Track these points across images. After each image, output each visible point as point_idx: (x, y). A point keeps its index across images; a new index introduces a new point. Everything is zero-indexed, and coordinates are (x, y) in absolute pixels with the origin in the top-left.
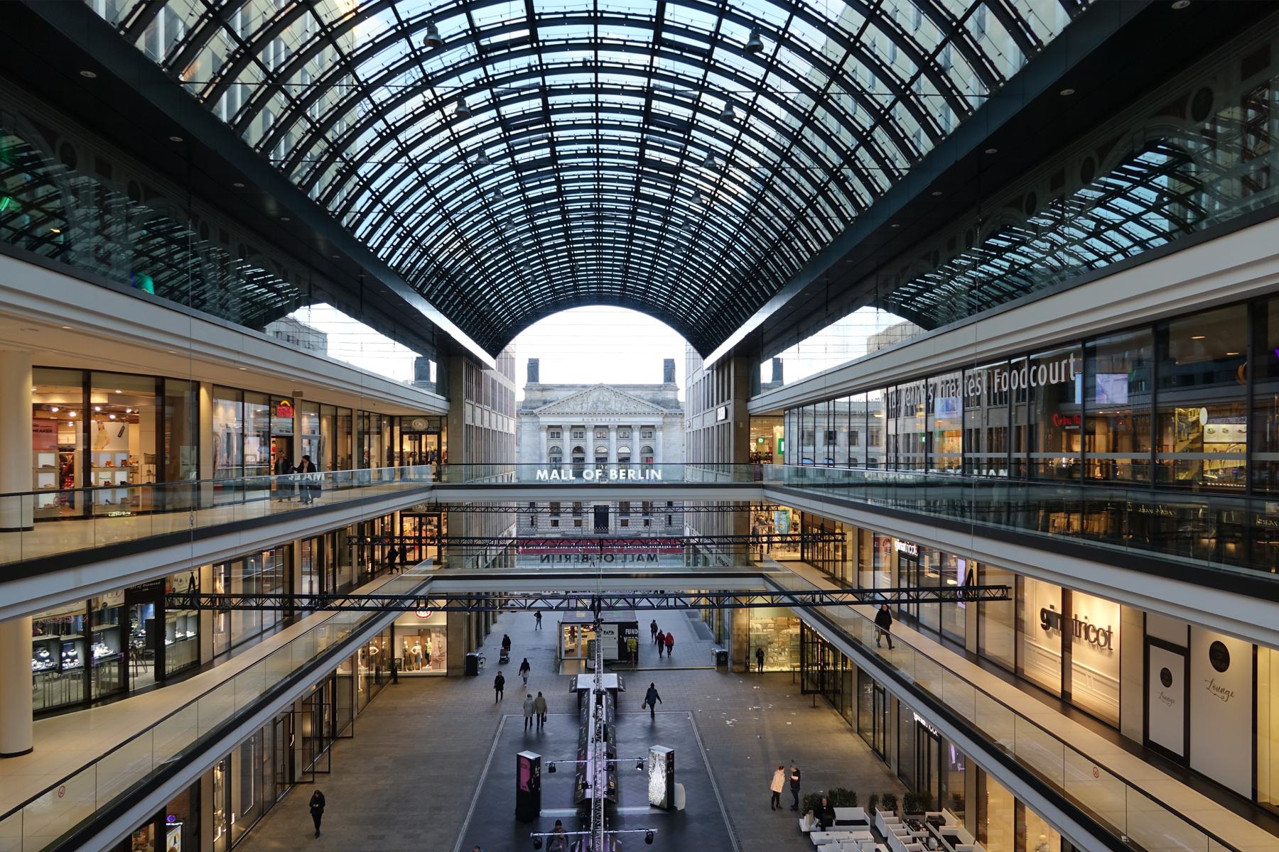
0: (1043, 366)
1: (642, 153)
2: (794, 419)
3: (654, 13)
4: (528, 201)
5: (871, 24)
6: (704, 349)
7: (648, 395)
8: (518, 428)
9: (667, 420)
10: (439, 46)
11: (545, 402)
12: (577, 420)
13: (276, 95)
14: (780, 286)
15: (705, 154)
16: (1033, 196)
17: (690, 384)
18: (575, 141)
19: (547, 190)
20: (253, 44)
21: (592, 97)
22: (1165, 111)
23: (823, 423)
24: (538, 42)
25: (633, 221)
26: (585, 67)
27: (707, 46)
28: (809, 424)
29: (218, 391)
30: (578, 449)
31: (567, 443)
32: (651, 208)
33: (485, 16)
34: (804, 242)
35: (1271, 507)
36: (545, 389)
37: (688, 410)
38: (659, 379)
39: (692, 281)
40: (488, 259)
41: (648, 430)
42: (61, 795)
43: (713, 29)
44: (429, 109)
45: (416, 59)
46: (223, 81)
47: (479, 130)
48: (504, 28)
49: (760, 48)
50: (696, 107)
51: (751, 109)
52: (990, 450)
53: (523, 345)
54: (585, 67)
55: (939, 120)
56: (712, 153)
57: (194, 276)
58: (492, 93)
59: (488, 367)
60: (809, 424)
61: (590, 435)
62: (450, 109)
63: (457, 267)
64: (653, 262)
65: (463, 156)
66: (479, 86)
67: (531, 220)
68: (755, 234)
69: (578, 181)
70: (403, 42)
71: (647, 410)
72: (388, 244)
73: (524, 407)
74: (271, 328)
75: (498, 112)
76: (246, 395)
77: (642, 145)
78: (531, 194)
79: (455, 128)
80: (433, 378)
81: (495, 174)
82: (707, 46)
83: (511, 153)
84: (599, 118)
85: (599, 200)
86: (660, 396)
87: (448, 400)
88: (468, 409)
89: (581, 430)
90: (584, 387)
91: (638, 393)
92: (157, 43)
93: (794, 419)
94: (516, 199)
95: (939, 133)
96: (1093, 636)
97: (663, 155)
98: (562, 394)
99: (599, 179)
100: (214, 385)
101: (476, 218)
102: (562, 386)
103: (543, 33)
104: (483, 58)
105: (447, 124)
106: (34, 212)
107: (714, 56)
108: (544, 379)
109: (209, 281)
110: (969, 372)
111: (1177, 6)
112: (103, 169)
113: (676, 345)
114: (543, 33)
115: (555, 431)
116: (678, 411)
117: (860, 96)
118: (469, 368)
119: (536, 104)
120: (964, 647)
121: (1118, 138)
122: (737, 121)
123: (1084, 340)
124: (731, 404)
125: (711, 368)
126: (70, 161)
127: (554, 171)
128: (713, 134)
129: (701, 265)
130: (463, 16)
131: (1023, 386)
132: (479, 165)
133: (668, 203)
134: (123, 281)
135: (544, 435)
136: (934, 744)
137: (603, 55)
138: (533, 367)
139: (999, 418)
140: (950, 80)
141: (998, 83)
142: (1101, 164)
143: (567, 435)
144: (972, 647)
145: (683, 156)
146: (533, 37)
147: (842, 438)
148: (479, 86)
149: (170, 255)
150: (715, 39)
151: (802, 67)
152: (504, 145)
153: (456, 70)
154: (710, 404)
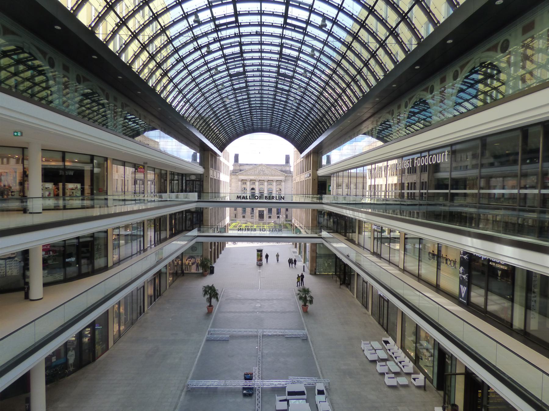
0: (434, 156)
1: (279, 71)
2: (335, 178)
3: (284, 12)
4: (234, 90)
5: (370, 15)
6: (301, 151)
7: (280, 168)
8: (28, 93)
10: (199, 23)
11: (241, 171)
12: (252, 177)
13: (134, 42)
14: (326, 130)
15: (303, 71)
17: (295, 164)
18: (253, 65)
19: (244, 97)
21: (260, 61)
22: (489, 50)
23: (346, 180)
25: (275, 99)
26: (257, 34)
28: (340, 180)
29: (116, 161)
30: (253, 189)
31: (248, 186)
32: (280, 104)
33: (218, 11)
34: (340, 107)
35: (547, 217)
37: (294, 174)
38: (284, 162)
39: (297, 123)
40: (221, 115)
41: (279, 182)
43: (307, 18)
44: (196, 50)
45: (191, 29)
47: (222, 78)
48: (225, 17)
49: (325, 26)
50: (300, 51)
51: (322, 52)
52: (408, 189)
53: (233, 148)
54: (257, 34)
56: (306, 70)
57: (103, 116)
59: (219, 156)
60: (340, 180)
61: (257, 183)
62: (204, 50)
63: (207, 116)
64: (284, 108)
65: (209, 70)
66: (215, 41)
67: (236, 97)
68: (322, 104)
69: (253, 78)
70: (185, 21)
71: (279, 174)
73: (233, 172)
74: (137, 139)
75: (223, 52)
76: (126, 164)
77: (279, 67)
78: (236, 87)
79: (206, 58)
80: (198, 160)
81: (222, 77)
83: (232, 85)
84: (261, 60)
85: (262, 90)
86: (284, 169)
87: (204, 168)
88: (211, 172)
90: (255, 165)
92: (85, 17)
93: (335, 178)
94: (233, 100)
96: (449, 262)
97: (287, 71)
98: (247, 167)
99: (262, 86)
100: (113, 159)
101: (215, 95)
102: (247, 164)
103: (241, 19)
104: (217, 29)
105: (203, 56)
106: (17, 78)
107: (308, 30)
108: (241, 161)
110: (431, 153)
111: (498, 3)
113: (289, 148)
114: (245, 55)
115: (244, 182)
116: (291, 175)
118: (212, 156)
119: (237, 49)
120: (398, 267)
122: (315, 57)
123: (451, 145)
124: (311, 172)
125: (303, 157)
127: (246, 91)
128: (300, 80)
129: (300, 116)
130: (209, 11)
131: (426, 164)
132: (222, 89)
133: (288, 91)
135: (240, 183)
136: (386, 303)
137: (264, 29)
138: (236, 157)
139: (413, 178)
140: (401, 39)
141: (421, 39)
142: (461, 72)
143: (248, 183)
144: (401, 267)
145: (294, 71)
146: (237, 21)
147: (353, 186)
148: (215, 41)
149: (99, 109)
150: (308, 22)
151: (338, 45)
153: (206, 34)
154: (302, 172)
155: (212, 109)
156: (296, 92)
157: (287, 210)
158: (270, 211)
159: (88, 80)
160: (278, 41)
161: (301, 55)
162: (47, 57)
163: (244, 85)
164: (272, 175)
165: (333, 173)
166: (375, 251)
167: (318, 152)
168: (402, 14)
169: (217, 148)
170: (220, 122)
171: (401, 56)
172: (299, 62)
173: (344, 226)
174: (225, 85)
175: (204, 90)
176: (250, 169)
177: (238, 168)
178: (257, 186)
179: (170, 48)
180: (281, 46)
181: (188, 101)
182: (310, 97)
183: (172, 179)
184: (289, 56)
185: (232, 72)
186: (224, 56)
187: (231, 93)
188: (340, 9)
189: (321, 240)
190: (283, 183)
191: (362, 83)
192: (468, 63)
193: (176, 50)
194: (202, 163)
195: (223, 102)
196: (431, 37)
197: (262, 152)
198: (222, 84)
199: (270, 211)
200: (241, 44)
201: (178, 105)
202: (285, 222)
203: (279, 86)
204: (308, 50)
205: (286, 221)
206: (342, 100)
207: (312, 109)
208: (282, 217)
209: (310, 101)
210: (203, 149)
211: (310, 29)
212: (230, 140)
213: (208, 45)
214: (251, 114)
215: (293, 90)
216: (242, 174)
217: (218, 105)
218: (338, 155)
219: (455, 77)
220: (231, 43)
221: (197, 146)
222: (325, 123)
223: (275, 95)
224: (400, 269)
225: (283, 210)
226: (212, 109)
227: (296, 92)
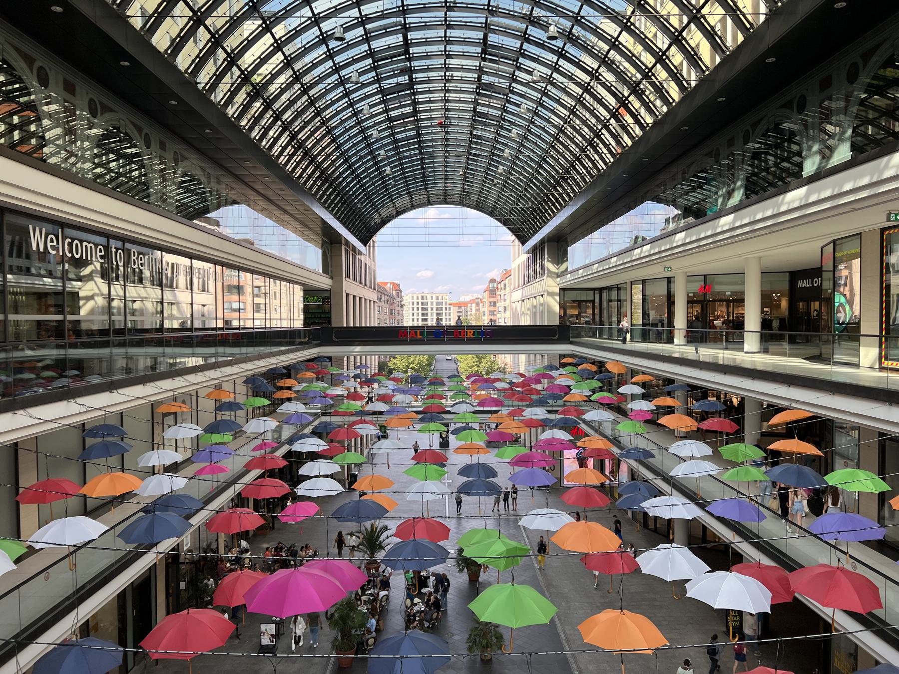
1: (479, 78)
6: (523, 240)
16: (718, 149)
20: (235, 55)
24: (409, 54)
42: (47, 579)
46: (200, 62)
55: (749, 17)
58: (365, 29)
59: (360, 253)
72: (285, 154)
77: (481, 70)
78: (393, 114)
95: (748, 26)
109: (52, 142)
112: (69, 88)
117: (631, 58)
119: (404, 79)
121: (761, 119)
125: (528, 252)
126: (44, 82)
134: (172, 212)
141: (704, 72)
142: (864, 66)
152: (374, 74)
159: (111, 110)
162: (36, 65)
163: (409, 110)
168: (692, 11)
169: (356, 237)
171: (693, 78)
172: (521, 60)
182: (543, 129)
185: (386, 84)
186: (371, 54)
192: (878, 46)
194: (326, 269)
196: (740, 48)
203: (480, 109)
206: (588, 156)
207: (561, 130)
209: (543, 134)
210: (331, 243)
214: (423, 168)
217: (358, 152)
219: (852, 78)
220: (385, 27)
221: (317, 234)
224: (609, 440)
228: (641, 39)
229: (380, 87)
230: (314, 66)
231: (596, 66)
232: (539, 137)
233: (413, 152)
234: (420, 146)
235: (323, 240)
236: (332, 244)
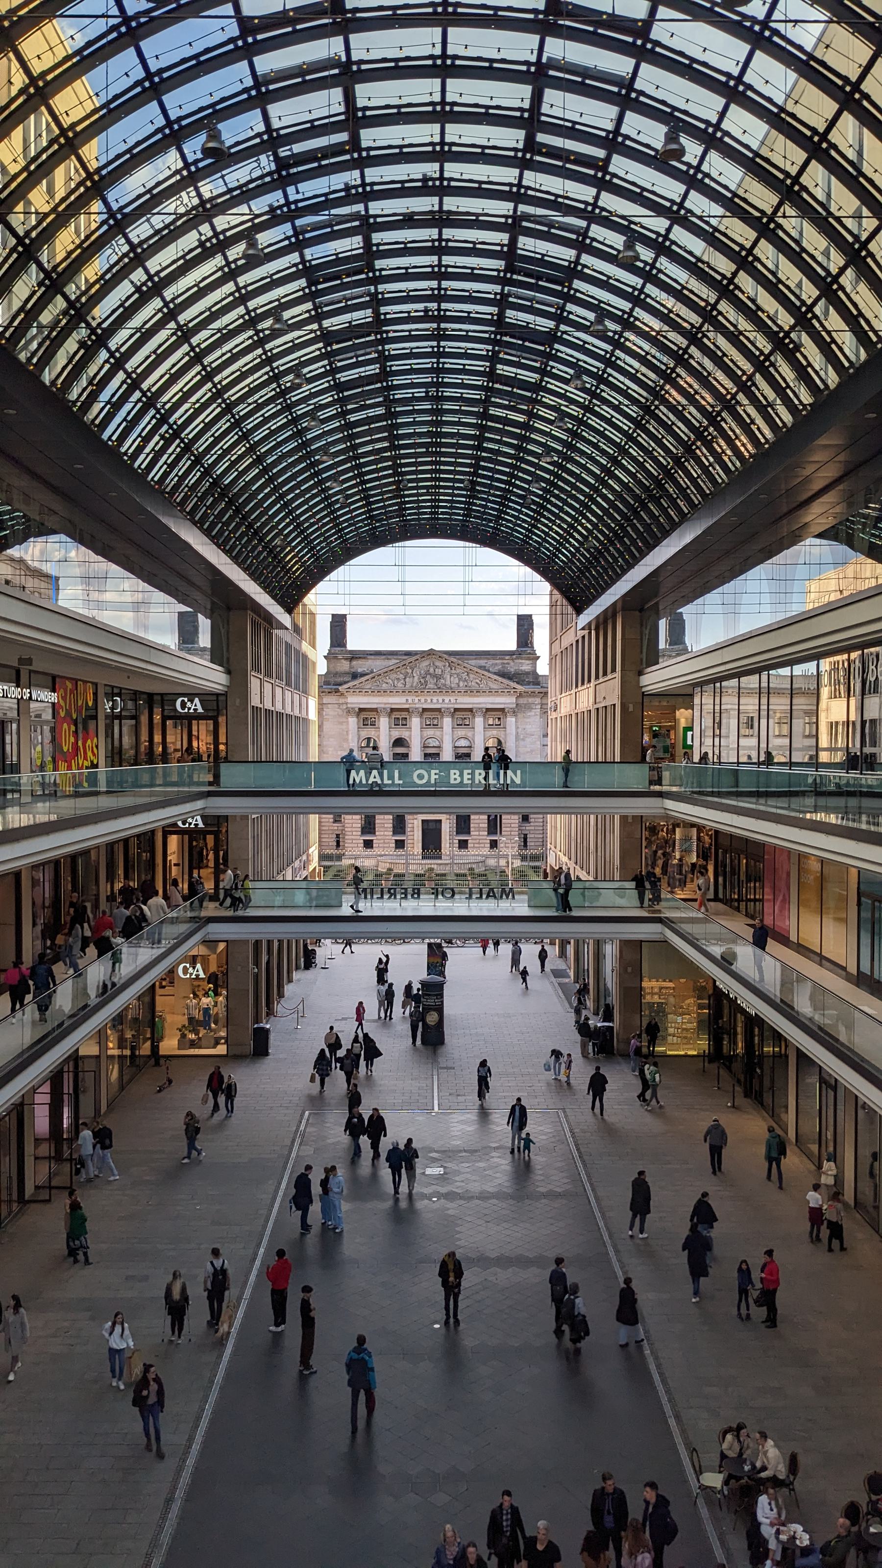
1: (501, 315)
2: (708, 700)
3: (526, 105)
7: (497, 664)
9: (522, 701)
11: (355, 676)
12: (397, 701)
15: (591, 316)
17: (557, 649)
18: (408, 299)
24: (374, 271)
27: (601, 153)
31: (384, 734)
36: (356, 656)
39: (565, 502)
43: (610, 126)
44: (206, 252)
49: (680, 153)
50: (582, 244)
58: (294, 227)
61: (415, 722)
62: (236, 252)
65: (252, 321)
66: (275, 218)
71: (494, 686)
73: (327, 683)
77: (502, 302)
80: (204, 640)
82: (601, 153)
85: (438, 385)
86: (513, 667)
87: (228, 672)
89: (404, 714)
90: (408, 654)
91: (482, 662)
93: (708, 700)
98: (377, 664)
99: (438, 371)
103: (369, 137)
104: (284, 176)
105: (231, 274)
107: (612, 169)
108: (353, 643)
115: (367, 717)
116: (537, 689)
119: (352, 244)
125: (588, 626)
129: (578, 477)
132: (275, 334)
135: (353, 721)
138: (339, 624)
143: (384, 722)
146: (355, 142)
148: (275, 218)
152: (309, 305)
155: (245, 436)
156: (549, 431)
157: (525, 818)
158: (463, 824)
160: (502, 208)
161: (586, 259)
164: (469, 692)
165: (701, 684)
166: (866, 968)
167: (643, 606)
170: (299, 525)
172: (577, 284)
173: (741, 875)
174: (286, 315)
175: (233, 394)
176: (388, 672)
177: (344, 666)
178: (415, 734)
179: (93, 217)
180: (514, 226)
181: (176, 434)
183: (121, 710)
184: (542, 261)
185: (333, 323)
187: (326, 399)
188: (761, 37)
189: (657, 928)
190: (511, 720)
191: (811, 352)
193: (97, 184)
194: (219, 654)
195: (300, 433)
197: (439, 599)
198: (295, 370)
199: (463, 824)
200: (367, 226)
201: (139, 450)
202: (518, 863)
204: (651, 133)
205: (524, 858)
208: (509, 844)
210: (225, 603)
211: (620, 165)
212: (320, 569)
213: (248, 235)
215: (554, 385)
216: (360, 691)
218: (713, 623)
222: (673, 502)
223: (481, 439)
225: (511, 822)
226: (245, 436)
227: (549, 431)
228: (797, 255)
229: (334, 379)
230: (201, 292)
231: (712, 297)
232: (609, 422)
233: (371, 413)
234: (391, 433)
235: (213, 603)
236: (229, 609)
